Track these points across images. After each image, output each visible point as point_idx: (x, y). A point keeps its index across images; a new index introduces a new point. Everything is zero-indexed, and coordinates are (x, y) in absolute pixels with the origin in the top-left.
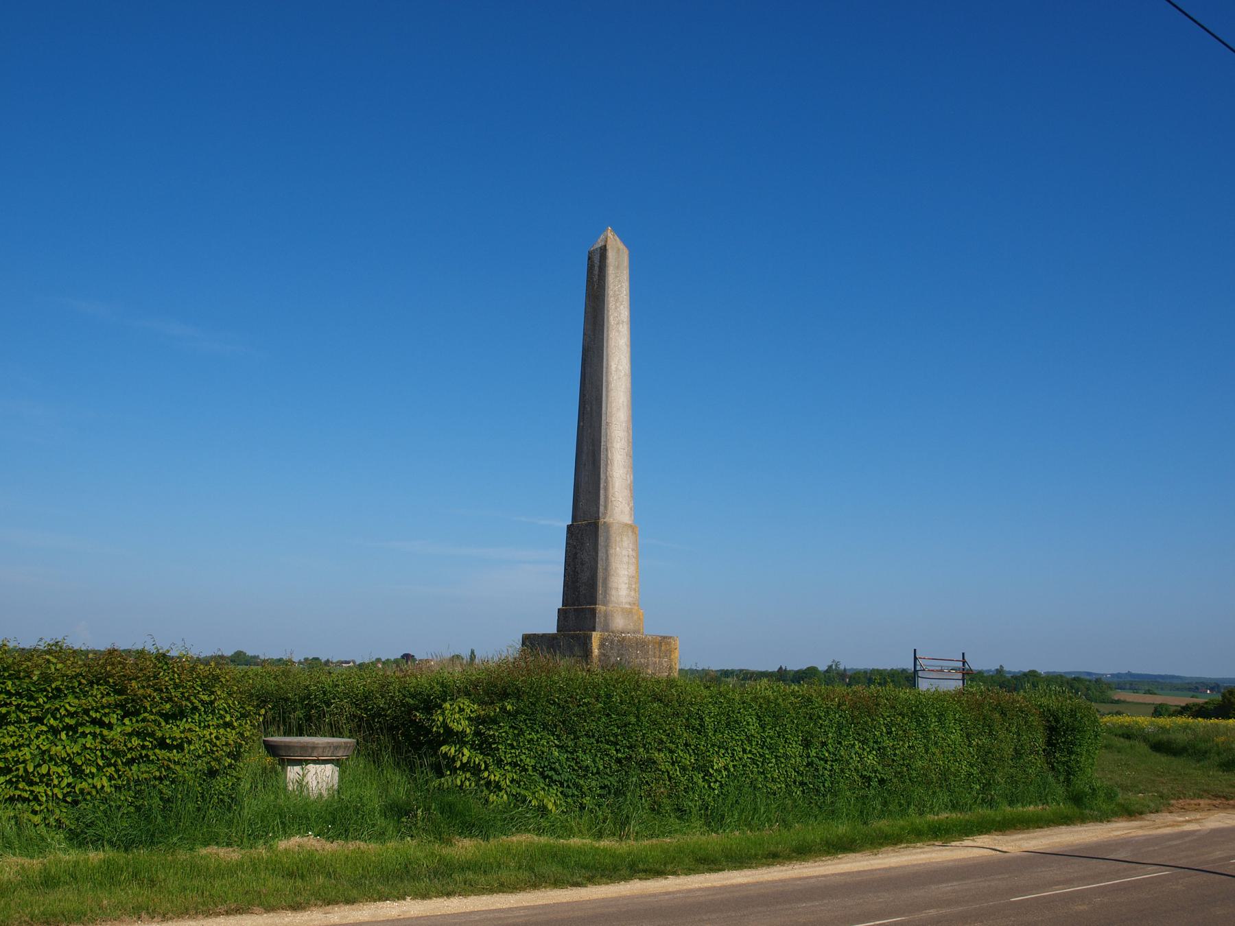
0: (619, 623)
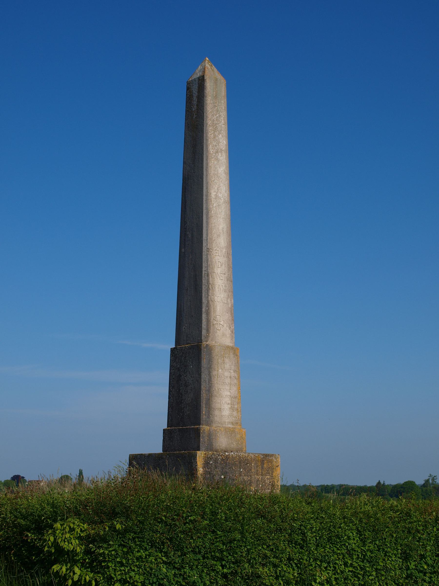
0: (222, 442)
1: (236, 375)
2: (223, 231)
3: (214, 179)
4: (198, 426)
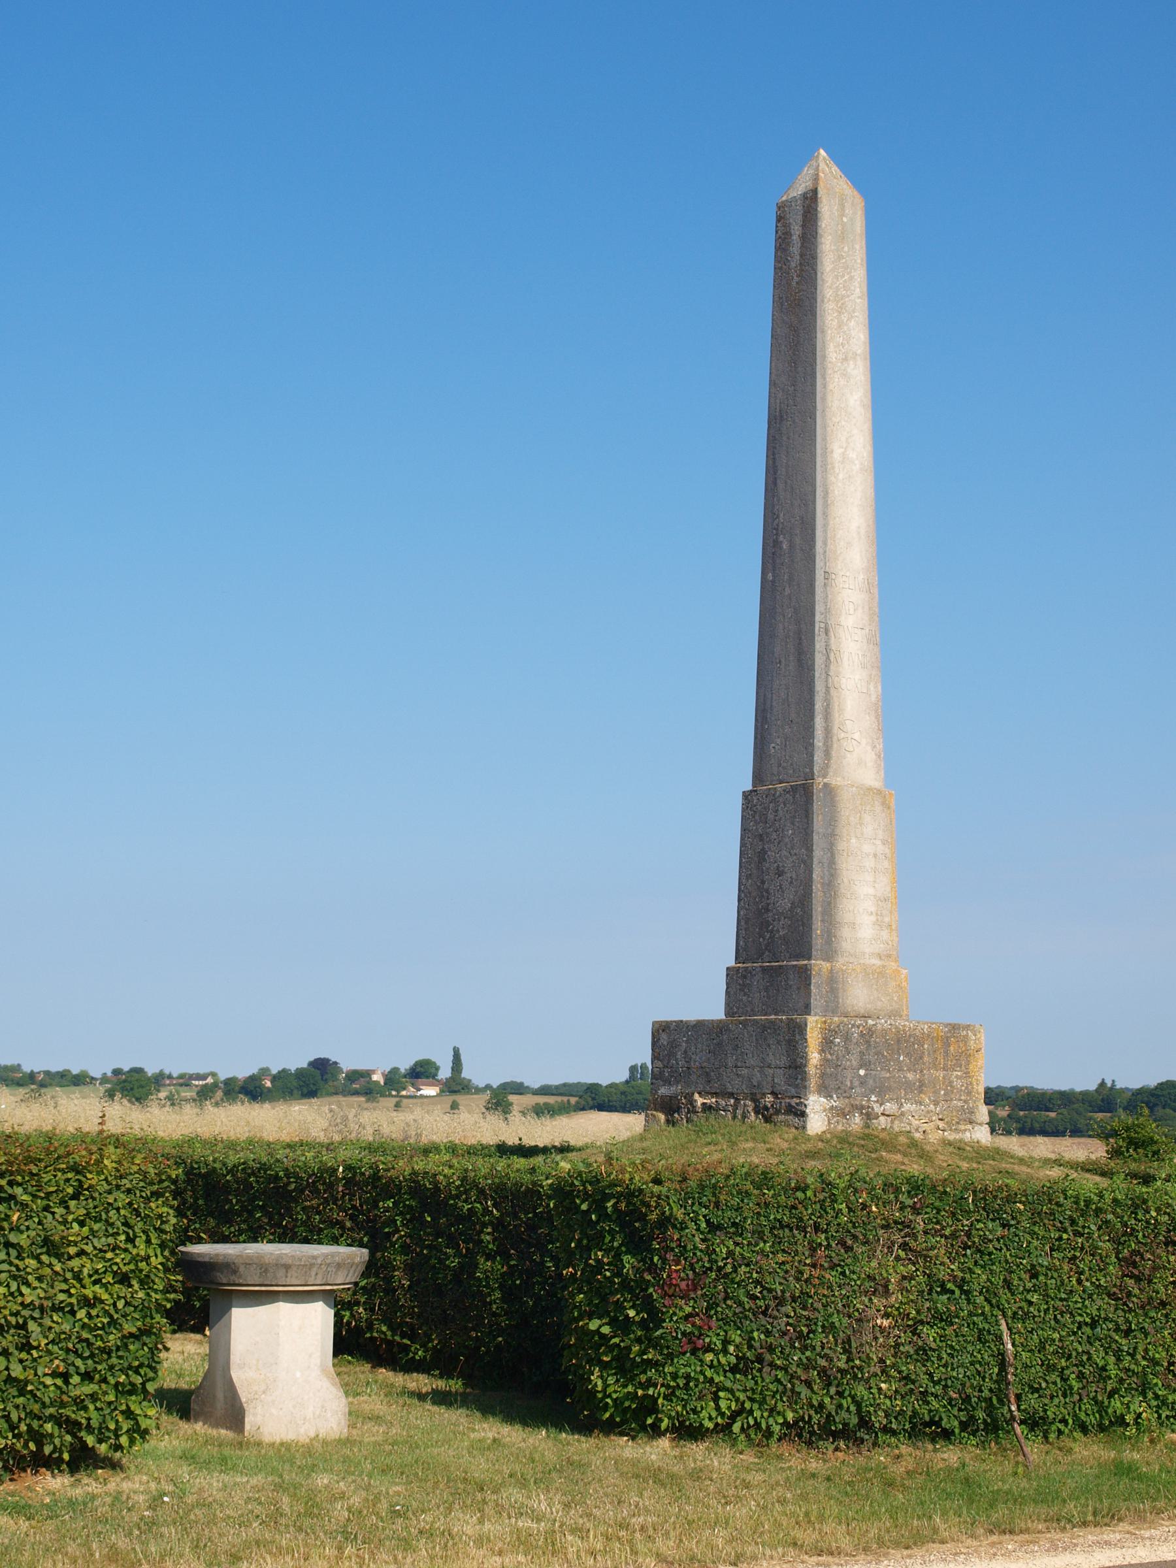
0: (859, 996)
1: (887, 851)
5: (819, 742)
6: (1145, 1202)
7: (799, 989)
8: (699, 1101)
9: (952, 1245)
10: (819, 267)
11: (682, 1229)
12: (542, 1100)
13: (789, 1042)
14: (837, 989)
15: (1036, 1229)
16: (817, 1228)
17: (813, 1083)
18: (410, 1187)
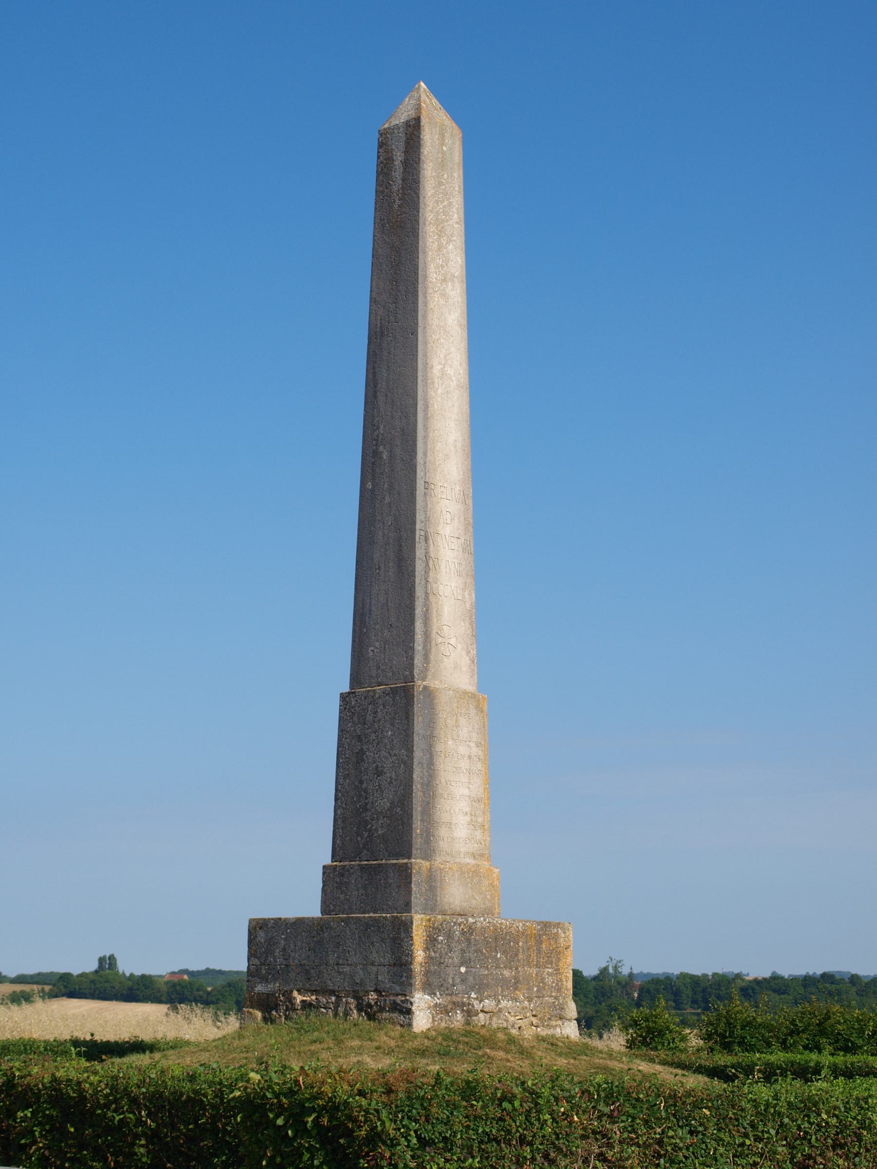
0: (455, 895)
1: (480, 753)
2: (455, 446)
3: (438, 336)
4: (406, 861)
5: (418, 647)
6: (815, 1104)
7: (399, 887)
8: (299, 998)
9: (645, 1154)
10: (421, 192)
11: (393, 1146)
12: (18, 988)
13: (394, 939)
14: (436, 888)
15: (722, 1135)
16: (522, 1140)
17: (418, 981)
18: (51, 1096)
